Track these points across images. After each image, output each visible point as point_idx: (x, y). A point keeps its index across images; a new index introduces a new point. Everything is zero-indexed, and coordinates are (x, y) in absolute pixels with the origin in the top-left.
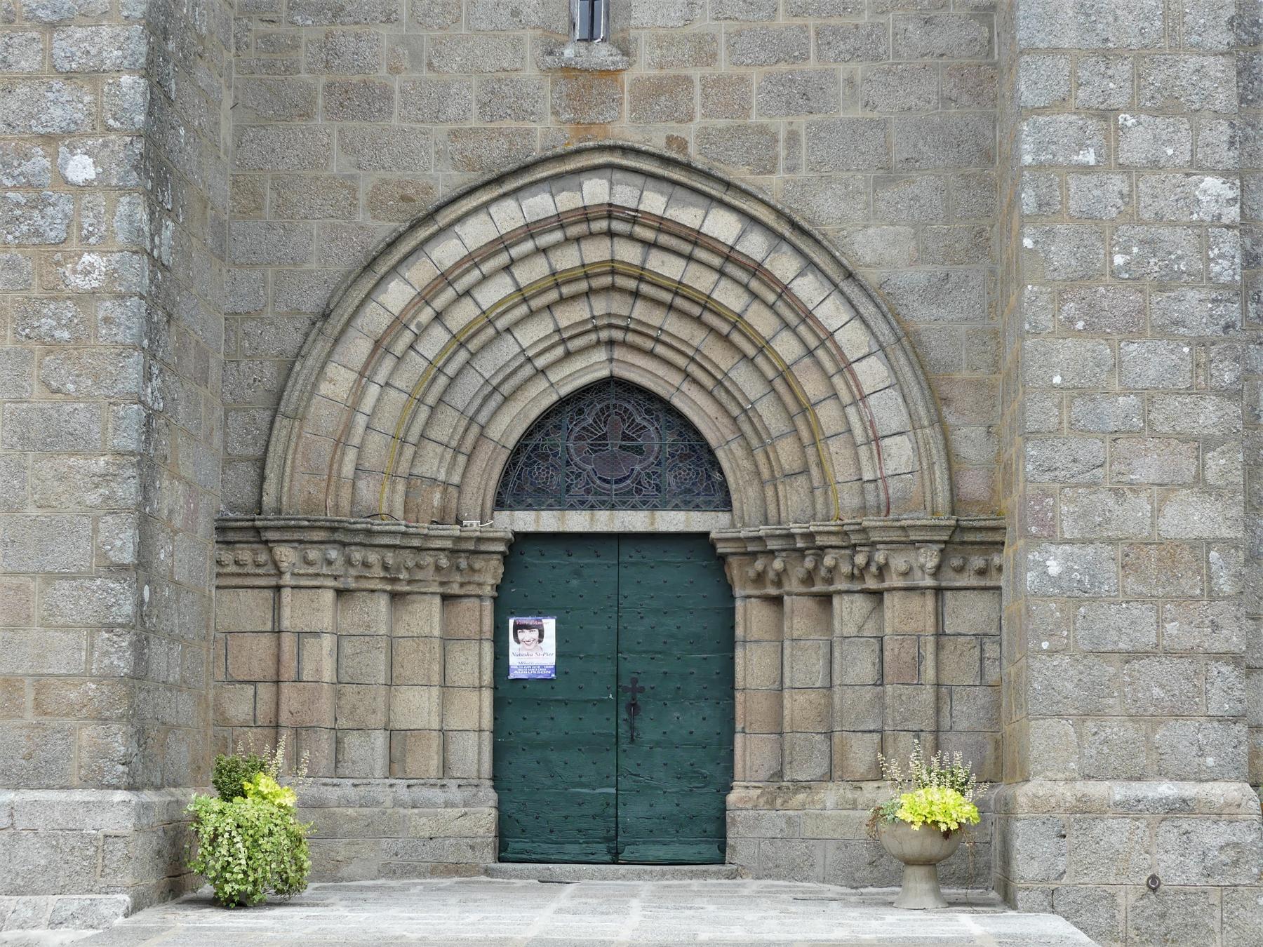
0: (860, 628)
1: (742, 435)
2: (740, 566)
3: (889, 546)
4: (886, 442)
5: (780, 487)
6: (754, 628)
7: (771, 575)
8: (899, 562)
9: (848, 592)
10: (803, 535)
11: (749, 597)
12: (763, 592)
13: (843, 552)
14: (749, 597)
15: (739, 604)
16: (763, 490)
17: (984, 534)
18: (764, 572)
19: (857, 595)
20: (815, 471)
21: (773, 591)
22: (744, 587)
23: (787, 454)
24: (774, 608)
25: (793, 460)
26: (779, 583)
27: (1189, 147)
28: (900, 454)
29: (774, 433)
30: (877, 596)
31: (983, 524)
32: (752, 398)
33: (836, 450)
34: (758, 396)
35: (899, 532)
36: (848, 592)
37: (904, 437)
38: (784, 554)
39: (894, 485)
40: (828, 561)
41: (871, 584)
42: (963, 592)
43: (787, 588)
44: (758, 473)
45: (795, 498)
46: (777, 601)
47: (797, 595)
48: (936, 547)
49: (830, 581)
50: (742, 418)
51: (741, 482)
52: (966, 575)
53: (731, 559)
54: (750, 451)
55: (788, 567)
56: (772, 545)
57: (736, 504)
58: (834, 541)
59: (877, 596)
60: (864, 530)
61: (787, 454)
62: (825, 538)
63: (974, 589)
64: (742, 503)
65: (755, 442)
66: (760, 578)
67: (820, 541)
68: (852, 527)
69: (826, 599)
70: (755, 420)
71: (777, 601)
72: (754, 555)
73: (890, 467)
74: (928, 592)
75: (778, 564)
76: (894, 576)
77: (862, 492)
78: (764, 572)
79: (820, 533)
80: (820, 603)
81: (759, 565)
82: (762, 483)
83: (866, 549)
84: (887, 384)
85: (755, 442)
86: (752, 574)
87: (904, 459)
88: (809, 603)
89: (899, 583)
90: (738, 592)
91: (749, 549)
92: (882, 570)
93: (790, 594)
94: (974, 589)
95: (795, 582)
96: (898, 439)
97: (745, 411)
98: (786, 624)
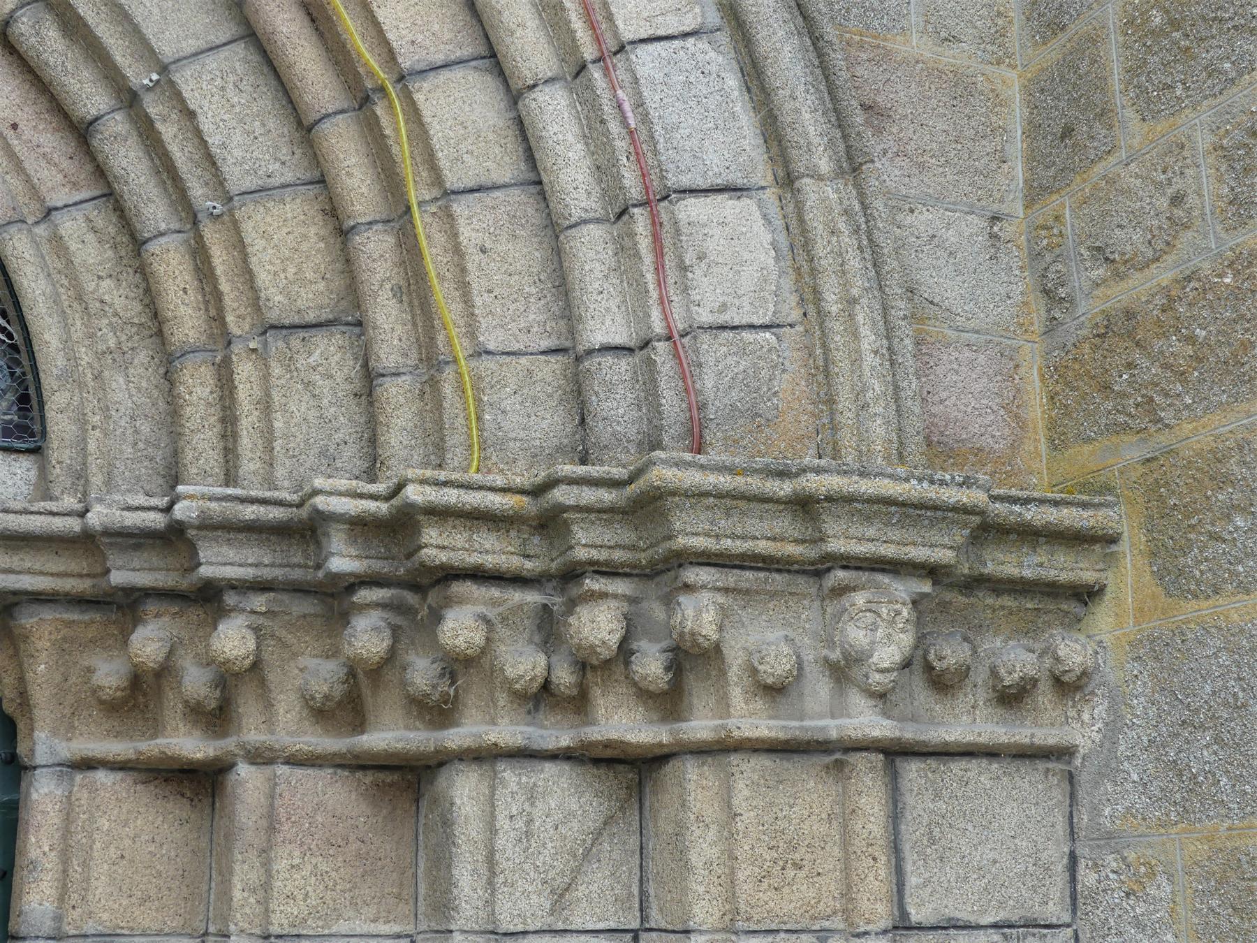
0: (560, 897)
1: (110, 194)
2: (63, 648)
3: (731, 578)
4: (691, 210)
5: (244, 370)
6: (100, 886)
7: (195, 681)
8: (767, 636)
9: (525, 755)
10: (360, 526)
11: (87, 765)
12: (150, 747)
13: (517, 596)
14: (87, 765)
15: (44, 795)
16: (169, 377)
17: (1041, 556)
18: (165, 672)
19: (550, 768)
20: (387, 316)
21: (190, 745)
22: (67, 728)
23: (282, 252)
24: (178, 809)
25: (300, 279)
26: (216, 716)
27: (660, 146)
28: (733, 255)
29: (237, 178)
30: (633, 773)
31: (1051, 515)
32: (166, 49)
33: (491, 249)
34: (190, 46)
35: (784, 524)
36: (525, 755)
37: (748, 204)
38: (259, 602)
39: (718, 367)
40: (461, 626)
41: (621, 722)
42: (957, 766)
43: (252, 732)
44: (156, 322)
45: (300, 407)
46: (200, 783)
47: (295, 761)
48: (903, 589)
49: (439, 712)
50: (117, 124)
51: (85, 356)
52: (964, 700)
53: (31, 621)
54: (134, 242)
55: (271, 654)
56: (220, 562)
57: (60, 424)
58: (492, 551)
59: (633, 773)
60: (647, 507)
61: (282, 252)
62: (460, 539)
63: (991, 753)
64: (82, 422)
65: (154, 212)
66: (141, 695)
67: (440, 547)
68: (589, 496)
69: (407, 782)
70: (169, 131)
71: (200, 783)
72: (126, 606)
73: (708, 297)
74: (859, 761)
75: (233, 639)
76: (736, 695)
77: (577, 397)
78: (165, 672)
79: (441, 514)
80: (377, 794)
81: (149, 640)
82: (169, 363)
83: (620, 587)
84: (689, 23)
85: (154, 212)
86: (109, 674)
87: (749, 278)
88: (333, 795)
89: (754, 722)
90: (45, 743)
91: (118, 578)
92: (691, 661)
93: (261, 757)
94: (991, 753)
95: (287, 711)
96: (728, 206)
97: (129, 99)
98: (244, 873)
